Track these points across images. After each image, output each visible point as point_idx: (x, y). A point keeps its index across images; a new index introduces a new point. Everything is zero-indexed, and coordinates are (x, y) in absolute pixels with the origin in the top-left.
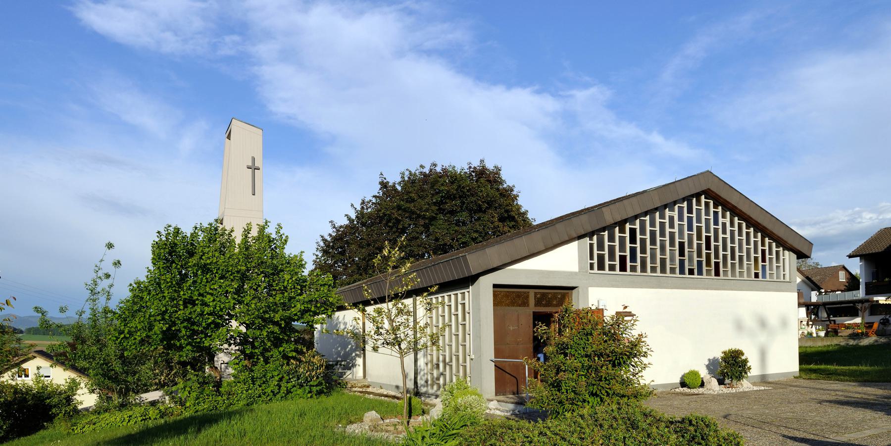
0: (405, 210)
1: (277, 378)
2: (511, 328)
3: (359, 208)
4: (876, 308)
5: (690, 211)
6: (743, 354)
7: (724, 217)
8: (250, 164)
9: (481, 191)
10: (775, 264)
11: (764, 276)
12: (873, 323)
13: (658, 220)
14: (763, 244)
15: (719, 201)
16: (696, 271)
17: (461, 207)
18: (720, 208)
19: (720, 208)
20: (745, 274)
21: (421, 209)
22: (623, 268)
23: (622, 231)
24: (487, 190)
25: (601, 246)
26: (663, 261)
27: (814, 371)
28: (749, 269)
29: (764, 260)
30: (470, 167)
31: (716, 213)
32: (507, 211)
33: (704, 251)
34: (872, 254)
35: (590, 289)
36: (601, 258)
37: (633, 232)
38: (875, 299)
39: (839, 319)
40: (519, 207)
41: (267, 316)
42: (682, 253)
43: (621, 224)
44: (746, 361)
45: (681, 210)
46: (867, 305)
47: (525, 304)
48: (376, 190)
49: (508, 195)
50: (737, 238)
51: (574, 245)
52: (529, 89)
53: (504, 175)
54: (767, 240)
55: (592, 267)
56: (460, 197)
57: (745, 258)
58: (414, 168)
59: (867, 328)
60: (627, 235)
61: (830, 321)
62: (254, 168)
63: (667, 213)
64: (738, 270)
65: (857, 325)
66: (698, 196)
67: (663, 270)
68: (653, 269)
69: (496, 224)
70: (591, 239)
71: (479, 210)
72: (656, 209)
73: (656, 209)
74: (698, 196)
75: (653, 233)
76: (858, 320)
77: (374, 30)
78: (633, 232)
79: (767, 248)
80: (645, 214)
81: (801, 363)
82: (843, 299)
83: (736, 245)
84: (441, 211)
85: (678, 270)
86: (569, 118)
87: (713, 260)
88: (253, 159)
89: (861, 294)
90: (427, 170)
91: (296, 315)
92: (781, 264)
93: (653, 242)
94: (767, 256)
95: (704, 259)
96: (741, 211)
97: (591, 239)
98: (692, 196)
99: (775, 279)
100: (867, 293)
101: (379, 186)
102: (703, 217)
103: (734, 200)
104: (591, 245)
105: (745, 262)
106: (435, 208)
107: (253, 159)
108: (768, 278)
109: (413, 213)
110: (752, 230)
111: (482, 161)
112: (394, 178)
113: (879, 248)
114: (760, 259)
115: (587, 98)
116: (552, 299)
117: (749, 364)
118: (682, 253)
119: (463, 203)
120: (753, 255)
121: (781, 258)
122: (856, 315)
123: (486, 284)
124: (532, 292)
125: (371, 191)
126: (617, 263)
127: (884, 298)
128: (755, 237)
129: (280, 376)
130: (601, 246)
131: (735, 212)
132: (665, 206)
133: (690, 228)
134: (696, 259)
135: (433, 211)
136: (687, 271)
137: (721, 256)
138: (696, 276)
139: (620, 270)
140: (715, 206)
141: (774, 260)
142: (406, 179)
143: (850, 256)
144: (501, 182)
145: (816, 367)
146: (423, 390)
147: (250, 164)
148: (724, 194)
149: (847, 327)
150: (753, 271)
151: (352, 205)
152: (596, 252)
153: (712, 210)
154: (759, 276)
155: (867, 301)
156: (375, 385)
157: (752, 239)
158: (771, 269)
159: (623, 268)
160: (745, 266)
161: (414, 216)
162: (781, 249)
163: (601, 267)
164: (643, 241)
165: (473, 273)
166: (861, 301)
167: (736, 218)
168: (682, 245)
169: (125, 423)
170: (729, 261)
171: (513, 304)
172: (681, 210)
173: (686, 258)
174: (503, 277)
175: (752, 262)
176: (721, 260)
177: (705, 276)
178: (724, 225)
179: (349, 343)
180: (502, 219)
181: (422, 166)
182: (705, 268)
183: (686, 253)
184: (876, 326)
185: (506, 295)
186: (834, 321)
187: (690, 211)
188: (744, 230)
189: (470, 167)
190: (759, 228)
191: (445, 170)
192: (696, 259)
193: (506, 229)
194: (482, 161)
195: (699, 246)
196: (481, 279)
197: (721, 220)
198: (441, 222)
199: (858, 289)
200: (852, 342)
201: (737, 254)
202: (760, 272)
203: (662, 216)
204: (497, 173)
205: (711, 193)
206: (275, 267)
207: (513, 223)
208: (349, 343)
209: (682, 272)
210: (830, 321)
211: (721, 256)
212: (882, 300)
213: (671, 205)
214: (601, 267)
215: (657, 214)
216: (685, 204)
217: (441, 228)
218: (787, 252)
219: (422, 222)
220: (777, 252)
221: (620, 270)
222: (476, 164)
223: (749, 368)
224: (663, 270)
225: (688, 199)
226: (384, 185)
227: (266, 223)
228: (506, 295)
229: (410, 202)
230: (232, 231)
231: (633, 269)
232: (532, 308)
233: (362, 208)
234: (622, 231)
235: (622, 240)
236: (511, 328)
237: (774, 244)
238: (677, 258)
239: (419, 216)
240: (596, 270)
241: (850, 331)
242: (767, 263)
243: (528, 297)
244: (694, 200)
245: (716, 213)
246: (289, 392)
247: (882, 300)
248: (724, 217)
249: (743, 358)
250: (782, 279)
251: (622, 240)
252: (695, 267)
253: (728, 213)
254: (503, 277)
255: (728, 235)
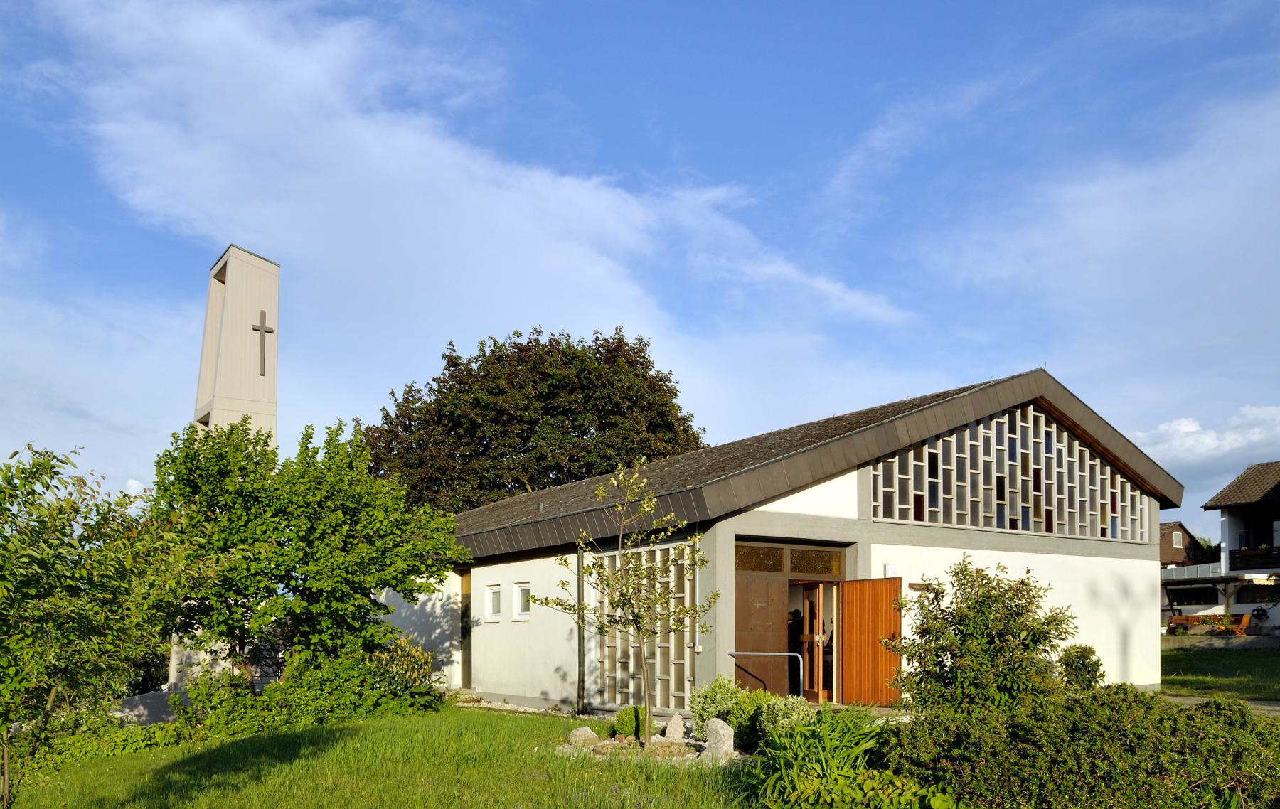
0: (487, 407)
1: (357, 682)
2: (758, 605)
3: (401, 400)
4: (1248, 592)
5: (1012, 430)
6: (1093, 653)
7: (1059, 440)
8: (258, 323)
9: (620, 380)
10: (1129, 517)
11: (1114, 535)
12: (1242, 616)
13: (968, 443)
14: (1113, 486)
15: (1054, 415)
16: (1020, 524)
17: (585, 405)
18: (1054, 425)
19: (1054, 425)
20: (1088, 530)
21: (516, 407)
22: (919, 516)
23: (918, 457)
24: (625, 378)
25: (888, 481)
26: (974, 505)
27: (1184, 684)
28: (1093, 522)
29: (1114, 510)
30: (597, 339)
31: (1048, 434)
32: (662, 415)
33: (1032, 493)
34: (1242, 505)
35: (873, 546)
36: (888, 498)
37: (933, 458)
38: (1248, 576)
39: (1187, 609)
40: (678, 408)
41: (357, 579)
42: (1001, 496)
43: (917, 447)
44: (1097, 664)
45: (1000, 425)
46: (1231, 587)
47: (777, 567)
48: (438, 368)
49: (660, 388)
50: (1077, 473)
51: (853, 476)
52: (597, 180)
53: (652, 353)
54: (1118, 478)
55: (875, 514)
56: (583, 388)
57: (1088, 505)
58: (504, 337)
59: (1232, 623)
60: (925, 463)
61: (1173, 610)
62: (263, 330)
63: (981, 431)
64: (1078, 524)
65: (1215, 617)
66: (1023, 407)
67: (975, 521)
68: (961, 519)
69: (645, 435)
70: (875, 469)
71: (617, 411)
72: (966, 426)
73: (966, 426)
74: (1023, 407)
75: (961, 462)
76: (1219, 610)
77: (323, 61)
78: (933, 458)
79: (1118, 490)
80: (951, 433)
81: (1164, 673)
82: (1181, 577)
83: (1076, 485)
84: (547, 411)
85: (994, 521)
86: (674, 240)
87: (1044, 507)
88: (263, 314)
89: (1223, 568)
90: (523, 341)
91: (394, 578)
92: (1138, 517)
93: (961, 477)
94: (1119, 504)
95: (1031, 504)
96: (1084, 431)
97: (875, 469)
98: (1016, 407)
99: (1129, 540)
100: (1232, 567)
101: (444, 363)
102: (1031, 440)
103: (1076, 416)
104: (875, 477)
105: (1088, 512)
106: (538, 405)
107: (263, 314)
108: (1119, 538)
109: (501, 412)
110: (1098, 462)
111: (618, 329)
112: (467, 352)
113: (1253, 495)
114: (1109, 508)
115: (694, 205)
116: (818, 559)
117: (1102, 669)
118: (1001, 496)
119: (587, 399)
120: (1099, 501)
121: (1138, 506)
122: (1214, 602)
123: (725, 533)
124: (787, 548)
125: (425, 374)
126: (911, 506)
127: (1266, 576)
128: (1102, 473)
129: (362, 678)
130: (888, 481)
131: (1076, 432)
132: (978, 422)
133: (1012, 457)
134: (1020, 504)
135: (536, 410)
136: (1007, 523)
137: (1055, 502)
138: (1019, 531)
139: (885, 516)
140: (1048, 424)
141: (1129, 509)
142: (488, 353)
143: (1207, 508)
144: (647, 365)
145: (1180, 678)
146: (596, 702)
147: (258, 323)
148: (1063, 406)
149: (1204, 621)
150: (1099, 527)
151: (392, 393)
152: (881, 489)
153: (1043, 429)
154: (1108, 535)
155: (1235, 580)
156: (492, 697)
157: (1098, 477)
158: (1123, 524)
159: (919, 516)
160: (1088, 518)
161: (500, 416)
162: (1138, 493)
163: (888, 512)
164: (947, 474)
165: (712, 517)
166: (1225, 580)
167: (1076, 443)
168: (1000, 481)
169: (118, 752)
170: (1066, 510)
171: (759, 567)
172: (1000, 425)
173: (1007, 502)
174: (748, 524)
175: (1098, 512)
176: (1054, 508)
177: (1032, 532)
178: (1059, 452)
179: (438, 625)
180: (653, 427)
181: (517, 334)
182: (1032, 519)
183: (1007, 495)
184: (1246, 620)
185: (756, 554)
186: (1180, 611)
187: (1012, 430)
188: (1088, 462)
189: (597, 339)
190: (1108, 458)
191: (554, 342)
192: (1020, 504)
193: (661, 444)
194: (618, 329)
195: (1025, 483)
196: (719, 524)
197: (1055, 445)
198: (542, 433)
199: (1218, 560)
200: (1219, 643)
201: (1077, 499)
202: (1108, 527)
203: (974, 437)
204: (640, 351)
205: (1048, 405)
206: (357, 498)
207: (669, 435)
208: (438, 625)
209: (1001, 524)
210: (1173, 610)
211: (1055, 502)
212: (1260, 578)
213: (985, 421)
214: (888, 512)
215: (967, 432)
216: (1006, 419)
217: (550, 439)
218: (1145, 498)
219: (518, 429)
220: (1133, 497)
221: (885, 516)
222: (608, 333)
223: (1102, 676)
224: (975, 521)
225: (1011, 411)
226: (452, 362)
227: (340, 426)
228: (756, 554)
229: (496, 394)
230: (269, 437)
231: (933, 516)
232: (787, 574)
233: (406, 399)
234: (918, 457)
235: (918, 470)
236: (758, 605)
237: (1128, 485)
238: (994, 502)
239: (512, 417)
240: (881, 518)
241: (1207, 628)
242: (1118, 515)
243: (781, 556)
244: (1019, 413)
245: (1048, 434)
246: (376, 705)
247: (1260, 578)
248: (1059, 440)
249: (1094, 658)
250: (1138, 540)
251: (918, 470)
252: (1019, 517)
253: (1065, 435)
254: (748, 524)
255: (1065, 469)
